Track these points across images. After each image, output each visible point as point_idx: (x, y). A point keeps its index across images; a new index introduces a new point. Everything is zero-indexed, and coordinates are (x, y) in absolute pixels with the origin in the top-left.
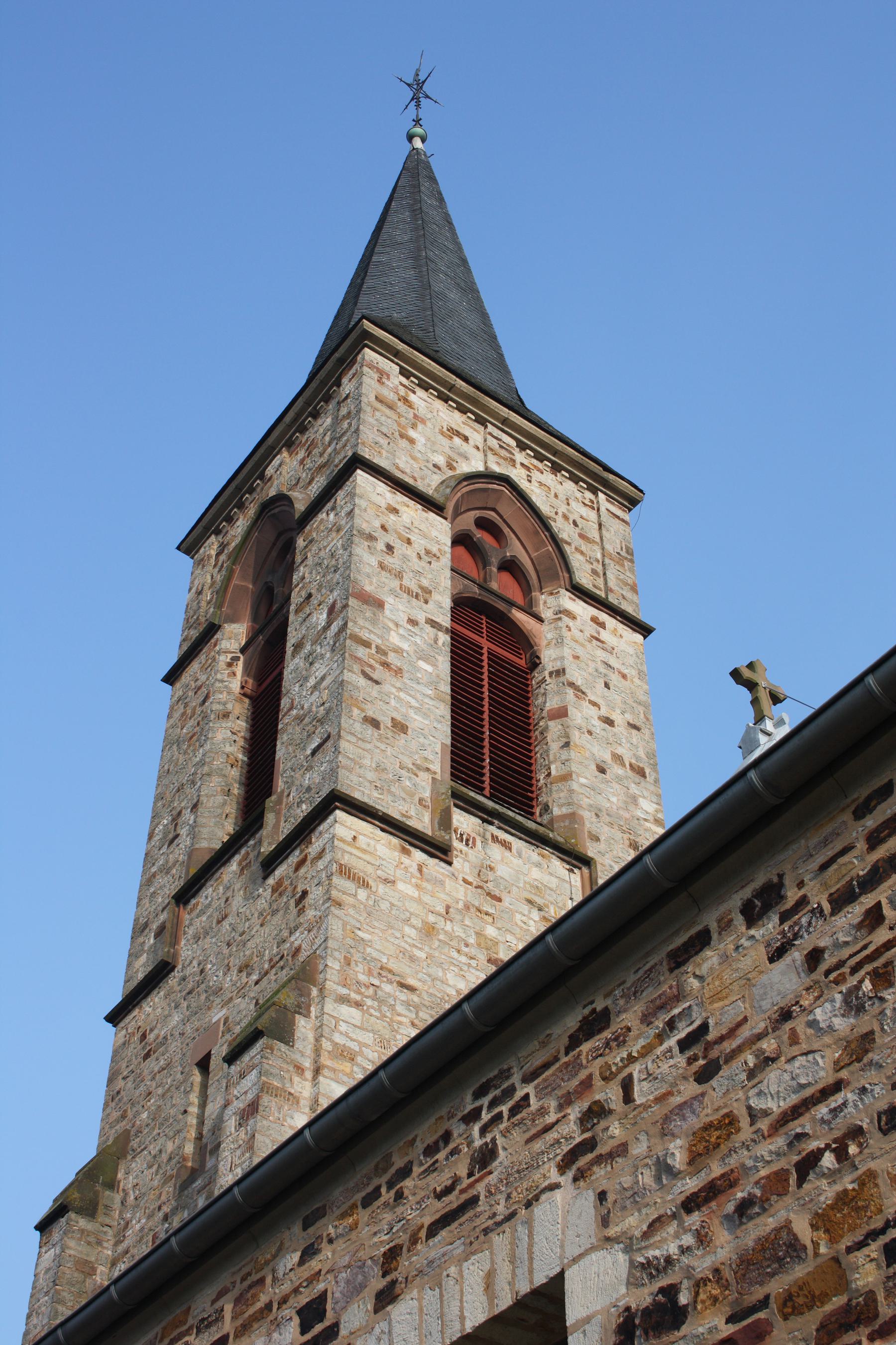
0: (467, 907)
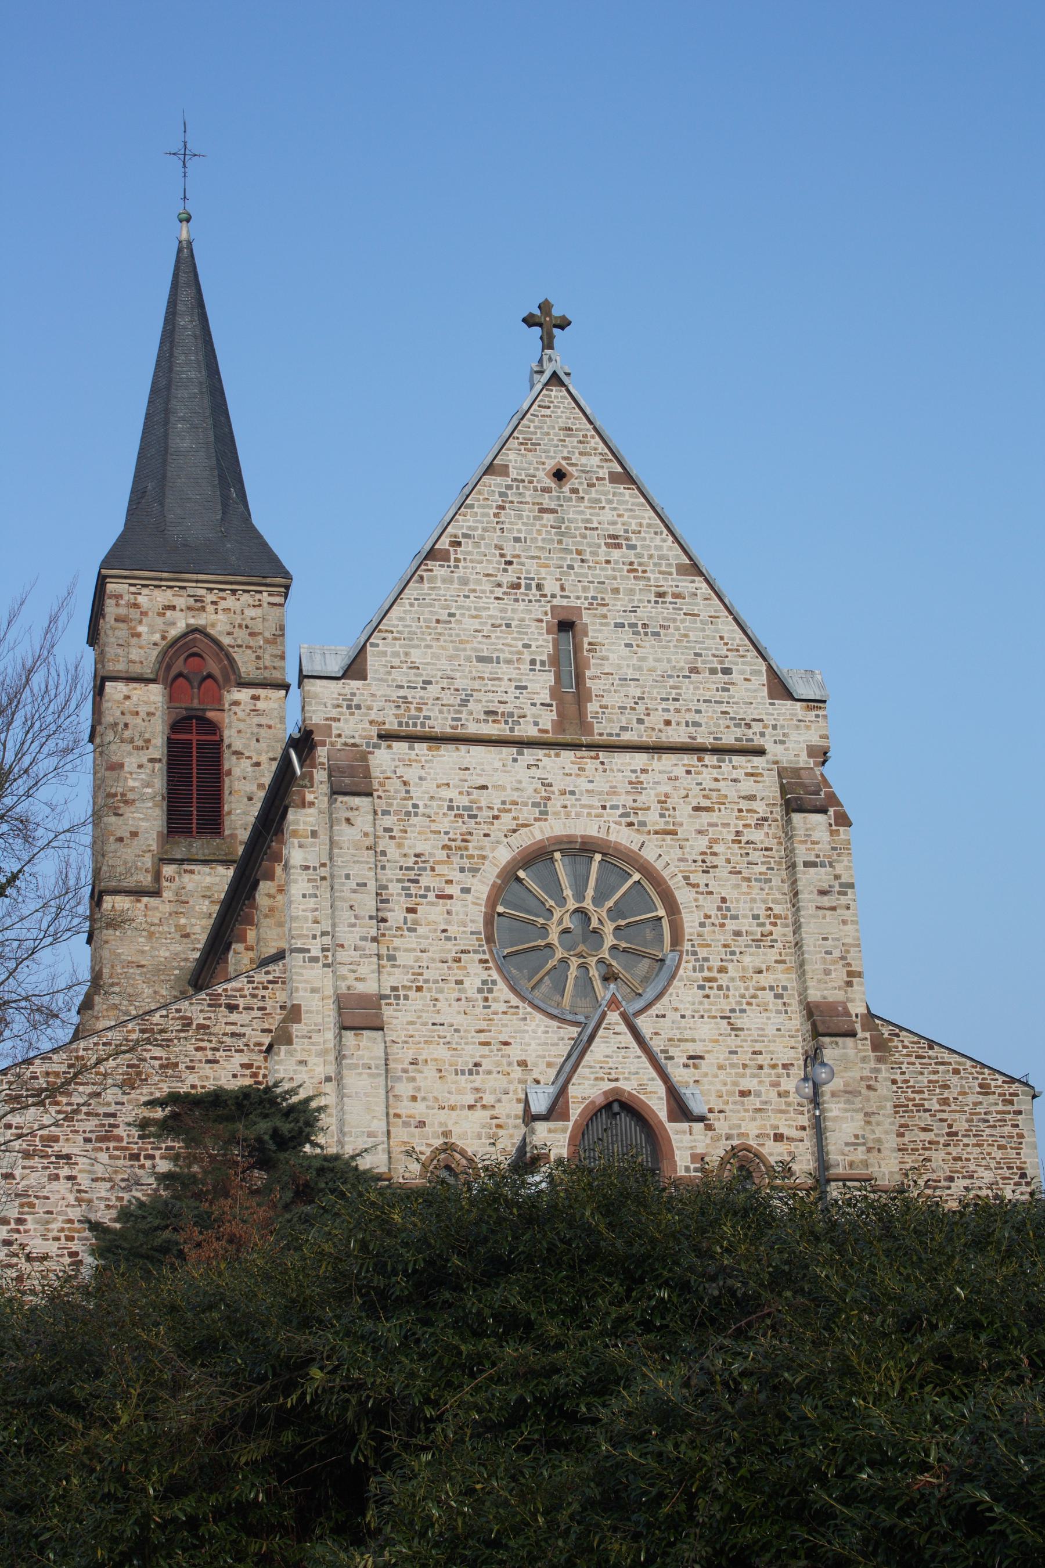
0: (170, 914)
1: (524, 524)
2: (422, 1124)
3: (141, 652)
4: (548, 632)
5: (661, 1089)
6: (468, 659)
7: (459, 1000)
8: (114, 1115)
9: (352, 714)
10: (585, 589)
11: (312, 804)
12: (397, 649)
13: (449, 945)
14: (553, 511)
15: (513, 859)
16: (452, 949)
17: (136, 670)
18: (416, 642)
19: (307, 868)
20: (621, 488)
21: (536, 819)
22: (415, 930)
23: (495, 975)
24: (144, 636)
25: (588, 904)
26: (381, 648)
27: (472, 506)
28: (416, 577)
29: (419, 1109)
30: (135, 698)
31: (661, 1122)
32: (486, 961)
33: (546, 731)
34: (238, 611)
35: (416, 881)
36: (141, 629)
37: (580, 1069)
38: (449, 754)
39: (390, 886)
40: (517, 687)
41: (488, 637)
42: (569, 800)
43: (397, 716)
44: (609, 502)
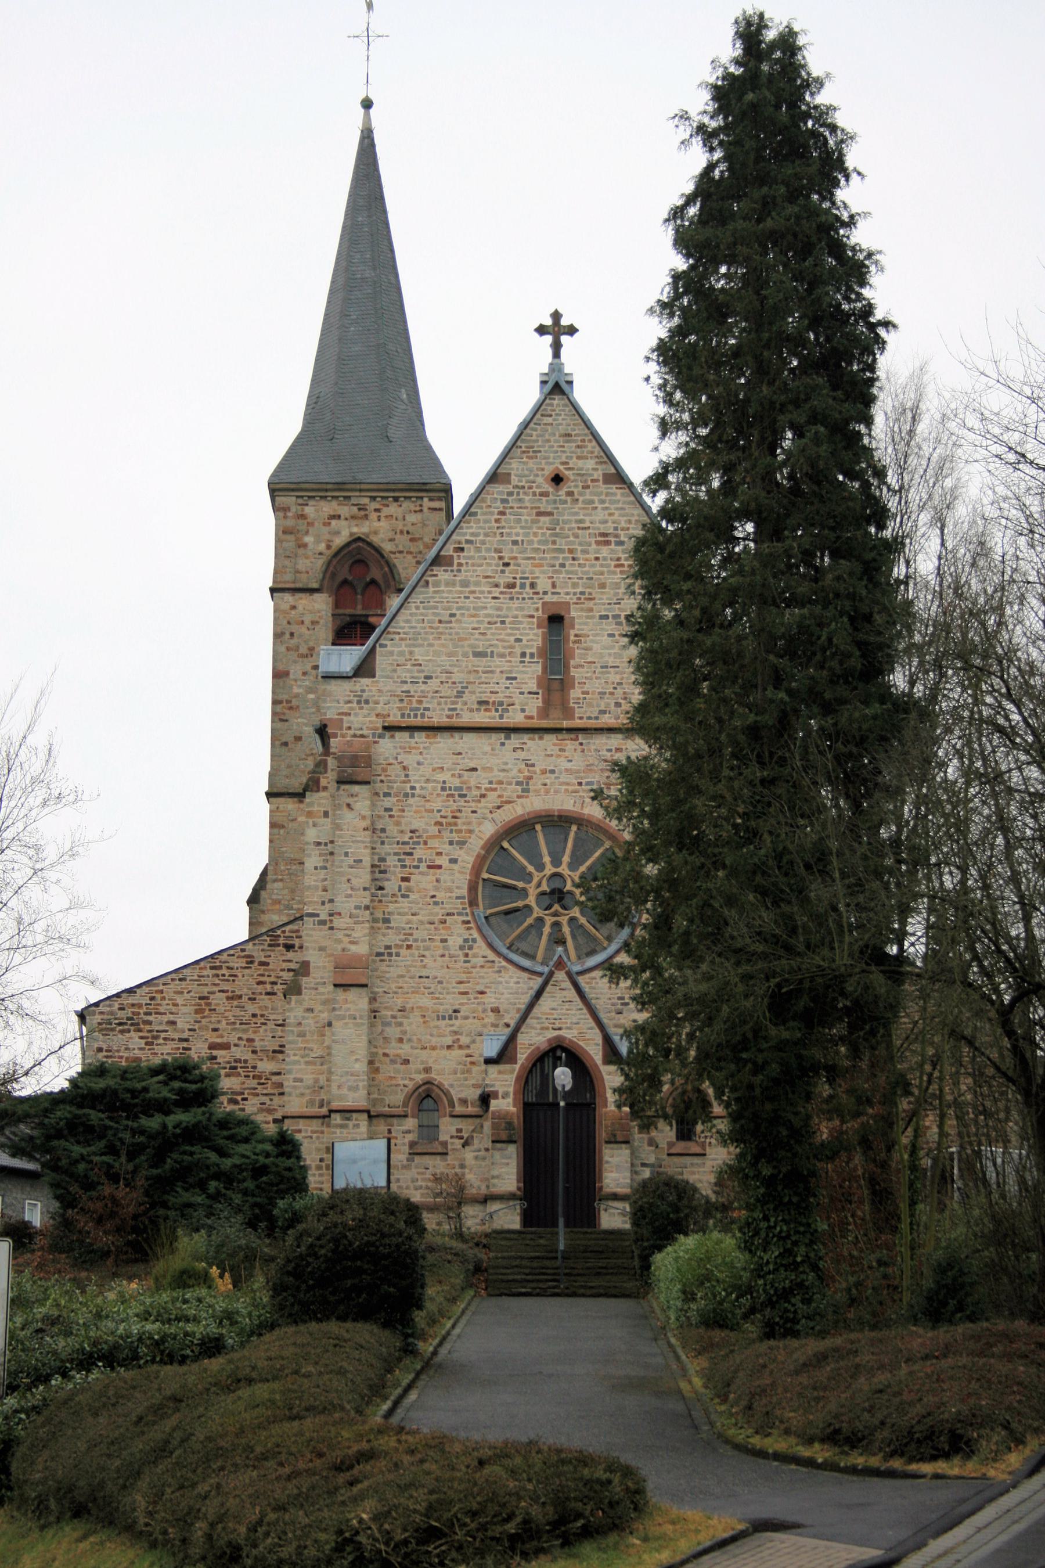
1: (522, 528)
2: (406, 1062)
3: (307, 561)
4: (539, 627)
5: (599, 1038)
6: (465, 655)
7: (443, 956)
8: (186, 1040)
9: (361, 708)
10: (575, 585)
11: (325, 788)
12: (403, 648)
13: (437, 909)
14: (550, 514)
15: (497, 832)
16: (439, 912)
17: (303, 581)
18: (420, 642)
19: (319, 844)
20: (613, 488)
21: (519, 797)
22: (407, 896)
23: (475, 934)
24: (311, 546)
25: (564, 869)
26: (389, 648)
27: (475, 514)
28: (422, 583)
29: (405, 1050)
30: (300, 608)
31: (596, 1065)
32: (468, 922)
33: (531, 718)
34: (400, 517)
35: (411, 854)
36: (309, 539)
37: (528, 1021)
38: (444, 743)
39: (388, 858)
40: (508, 678)
41: (484, 634)
42: (549, 779)
43: (400, 709)
44: (602, 502)
